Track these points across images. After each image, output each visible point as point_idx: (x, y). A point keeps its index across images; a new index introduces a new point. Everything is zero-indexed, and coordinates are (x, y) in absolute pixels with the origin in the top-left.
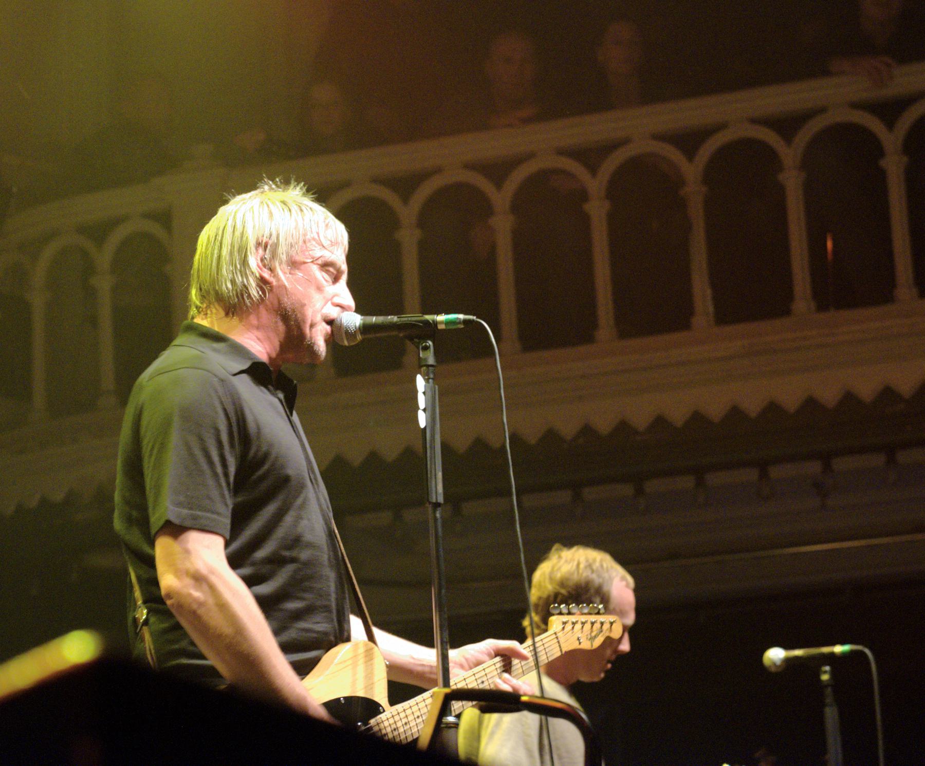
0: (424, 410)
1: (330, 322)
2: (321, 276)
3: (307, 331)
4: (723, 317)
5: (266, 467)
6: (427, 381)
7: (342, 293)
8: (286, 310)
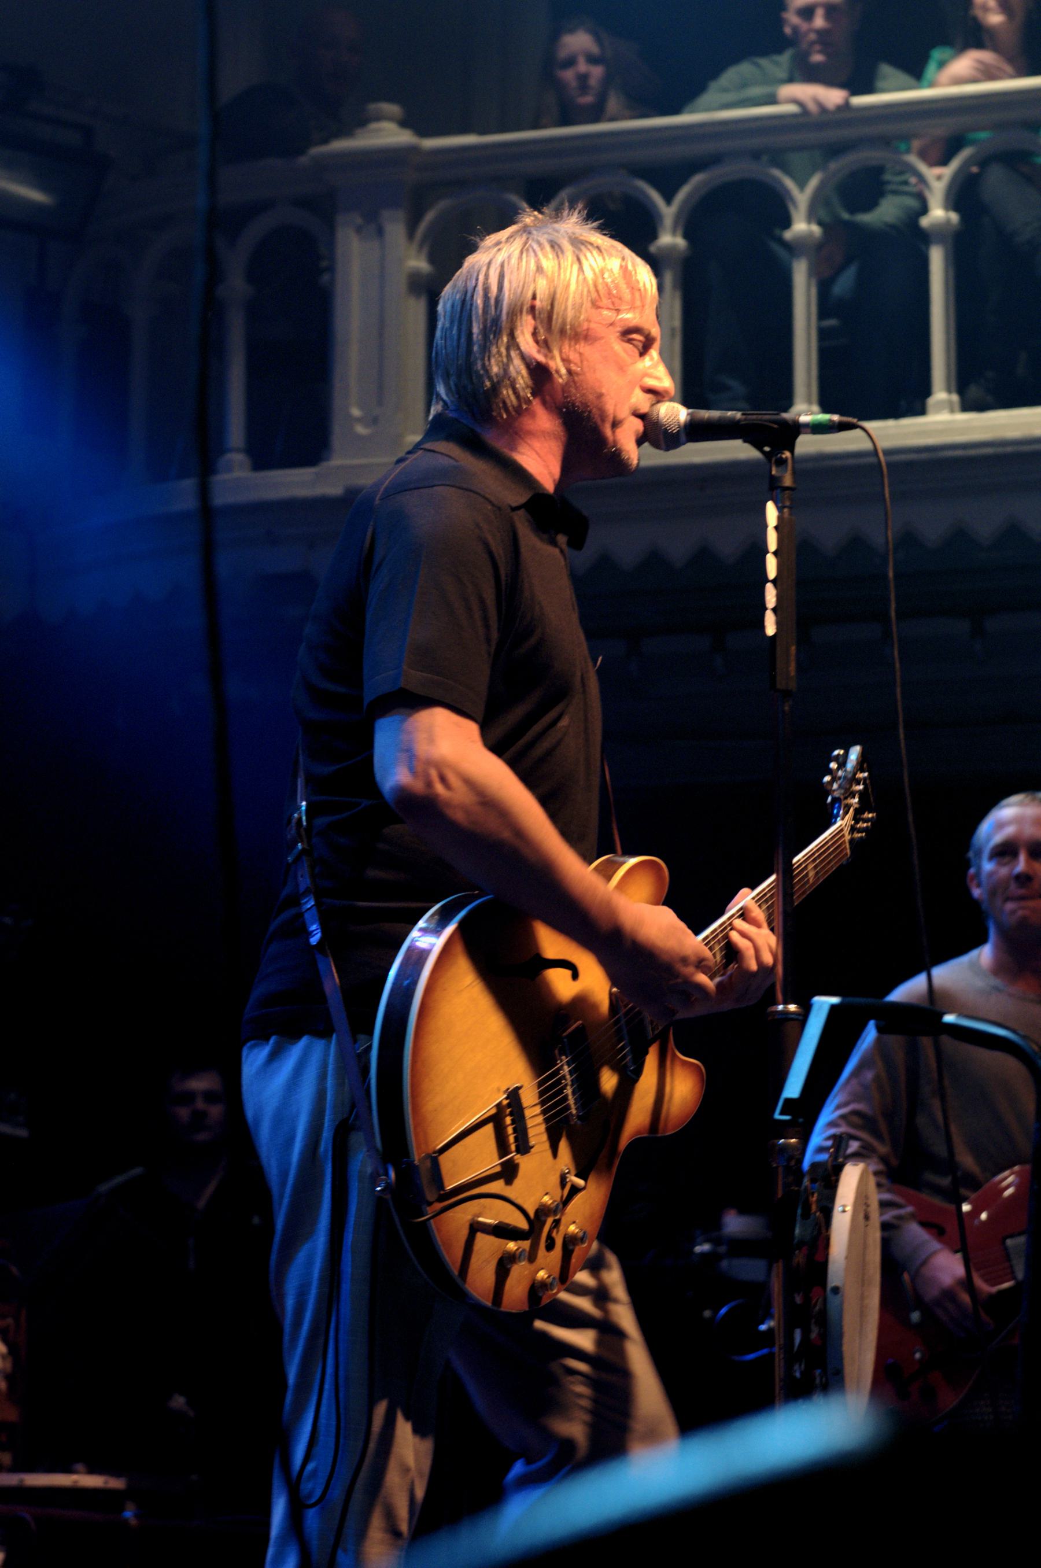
0: (775, 553)
1: (642, 417)
2: (619, 348)
3: (608, 432)
4: (596, 869)
5: (533, 640)
6: (780, 509)
7: (657, 371)
8: (573, 405)
